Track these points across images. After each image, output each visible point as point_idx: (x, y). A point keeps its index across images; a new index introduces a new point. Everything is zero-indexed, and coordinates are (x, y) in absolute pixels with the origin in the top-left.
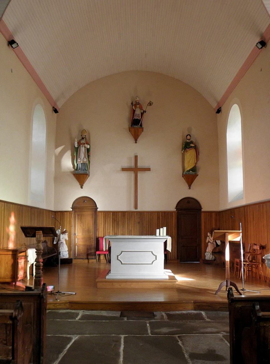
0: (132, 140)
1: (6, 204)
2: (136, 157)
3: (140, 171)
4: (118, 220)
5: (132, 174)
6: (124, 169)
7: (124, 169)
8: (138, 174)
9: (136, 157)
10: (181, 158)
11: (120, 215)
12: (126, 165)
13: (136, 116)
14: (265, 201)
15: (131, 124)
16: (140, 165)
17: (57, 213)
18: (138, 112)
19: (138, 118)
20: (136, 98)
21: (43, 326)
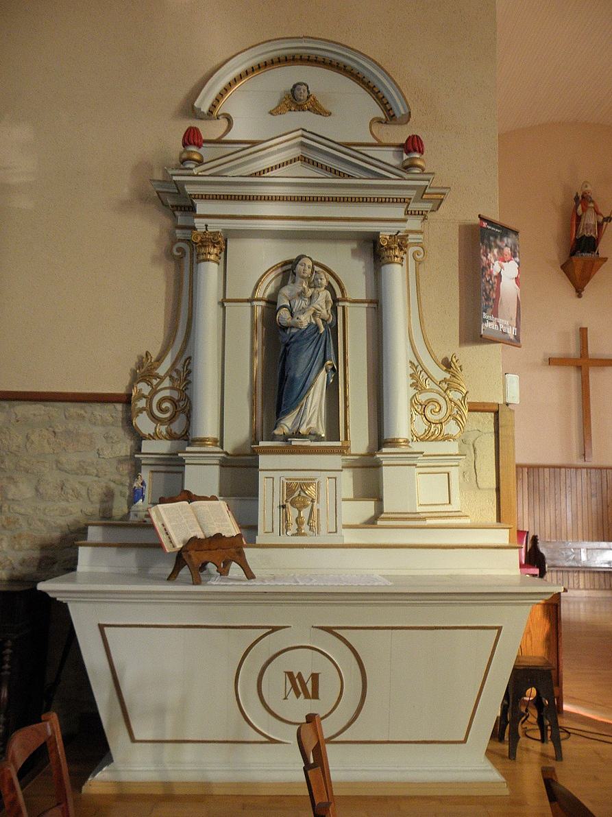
0: (567, 288)
1: (552, 470)
2: (583, 332)
3: (594, 366)
4: (541, 488)
5: (573, 376)
6: (552, 362)
7: (552, 362)
8: (590, 375)
9: (583, 332)
10: (254, 240)
11: (547, 475)
12: (556, 351)
13: (589, 230)
14: (383, 291)
15: (569, 255)
16: (593, 351)
17: (536, 470)
18: (590, 219)
19: (594, 236)
20: (586, 186)
21: (196, 288)
